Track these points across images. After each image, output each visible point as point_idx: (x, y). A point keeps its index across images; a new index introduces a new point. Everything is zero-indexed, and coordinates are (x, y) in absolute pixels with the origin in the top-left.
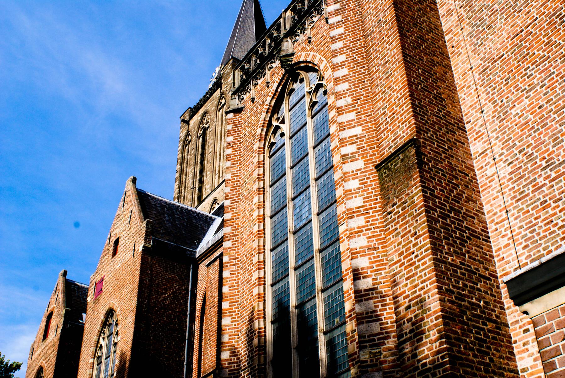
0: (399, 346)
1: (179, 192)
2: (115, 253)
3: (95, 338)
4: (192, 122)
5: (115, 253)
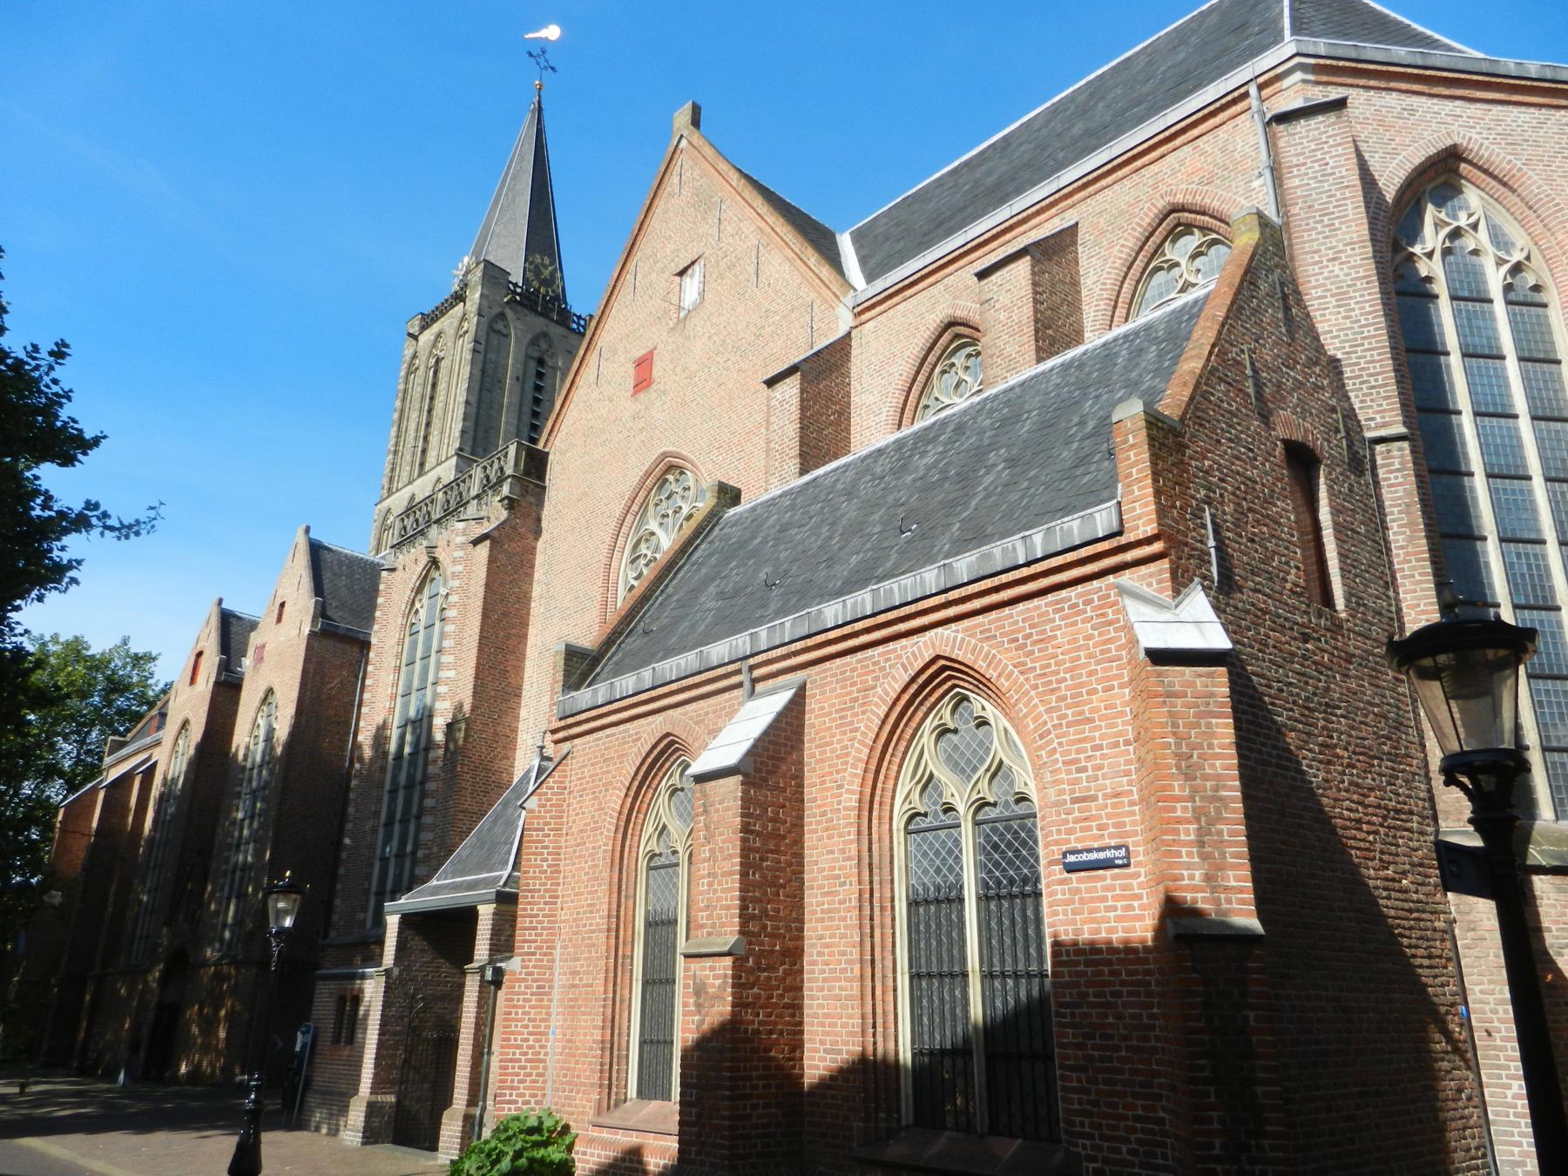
0: (216, 1012)
1: (397, 444)
2: (279, 620)
3: (252, 714)
4: (422, 338)
5: (279, 620)
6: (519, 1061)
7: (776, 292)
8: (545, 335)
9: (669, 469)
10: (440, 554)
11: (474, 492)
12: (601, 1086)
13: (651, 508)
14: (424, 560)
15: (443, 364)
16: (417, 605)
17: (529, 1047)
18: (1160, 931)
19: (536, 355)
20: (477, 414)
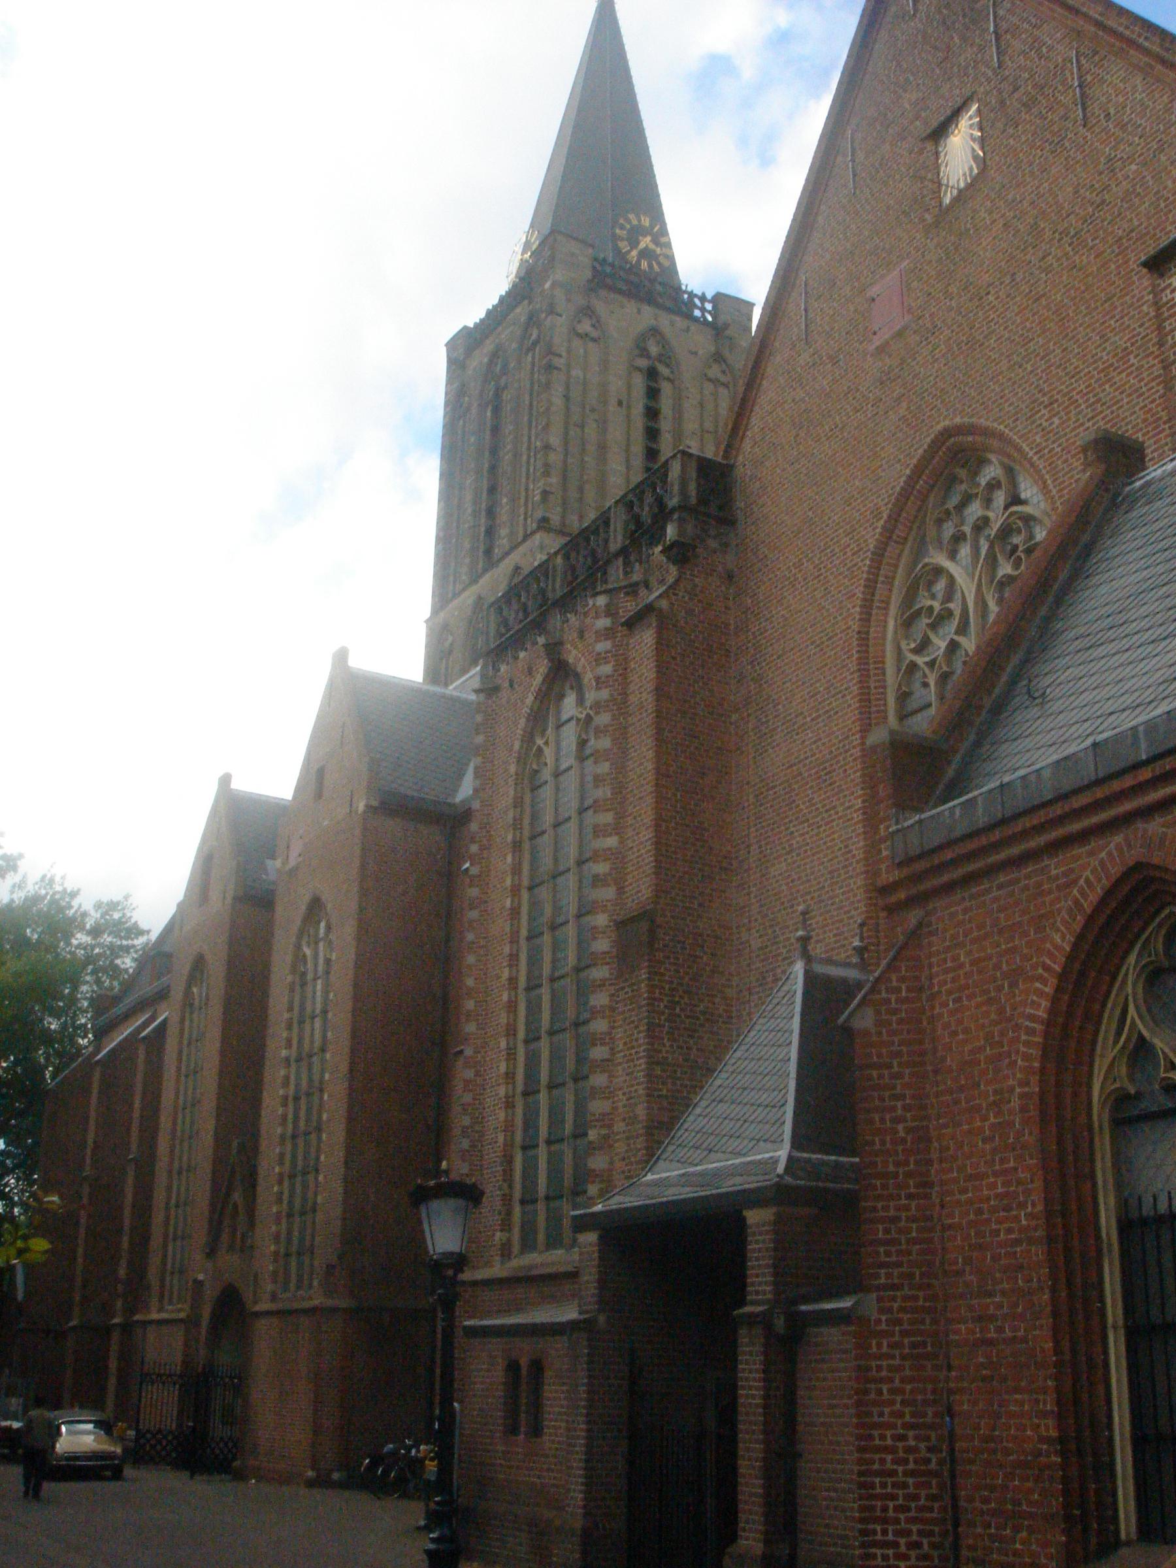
6: (893, 1473)
7: (1123, 127)
8: (655, 331)
9: (953, 461)
10: (573, 655)
11: (615, 544)
12: (1068, 1518)
13: (932, 532)
14: (542, 668)
15: (506, 396)
16: (540, 742)
17: (908, 1450)
18: (294, 797)
19: (643, 363)
20: (565, 462)
